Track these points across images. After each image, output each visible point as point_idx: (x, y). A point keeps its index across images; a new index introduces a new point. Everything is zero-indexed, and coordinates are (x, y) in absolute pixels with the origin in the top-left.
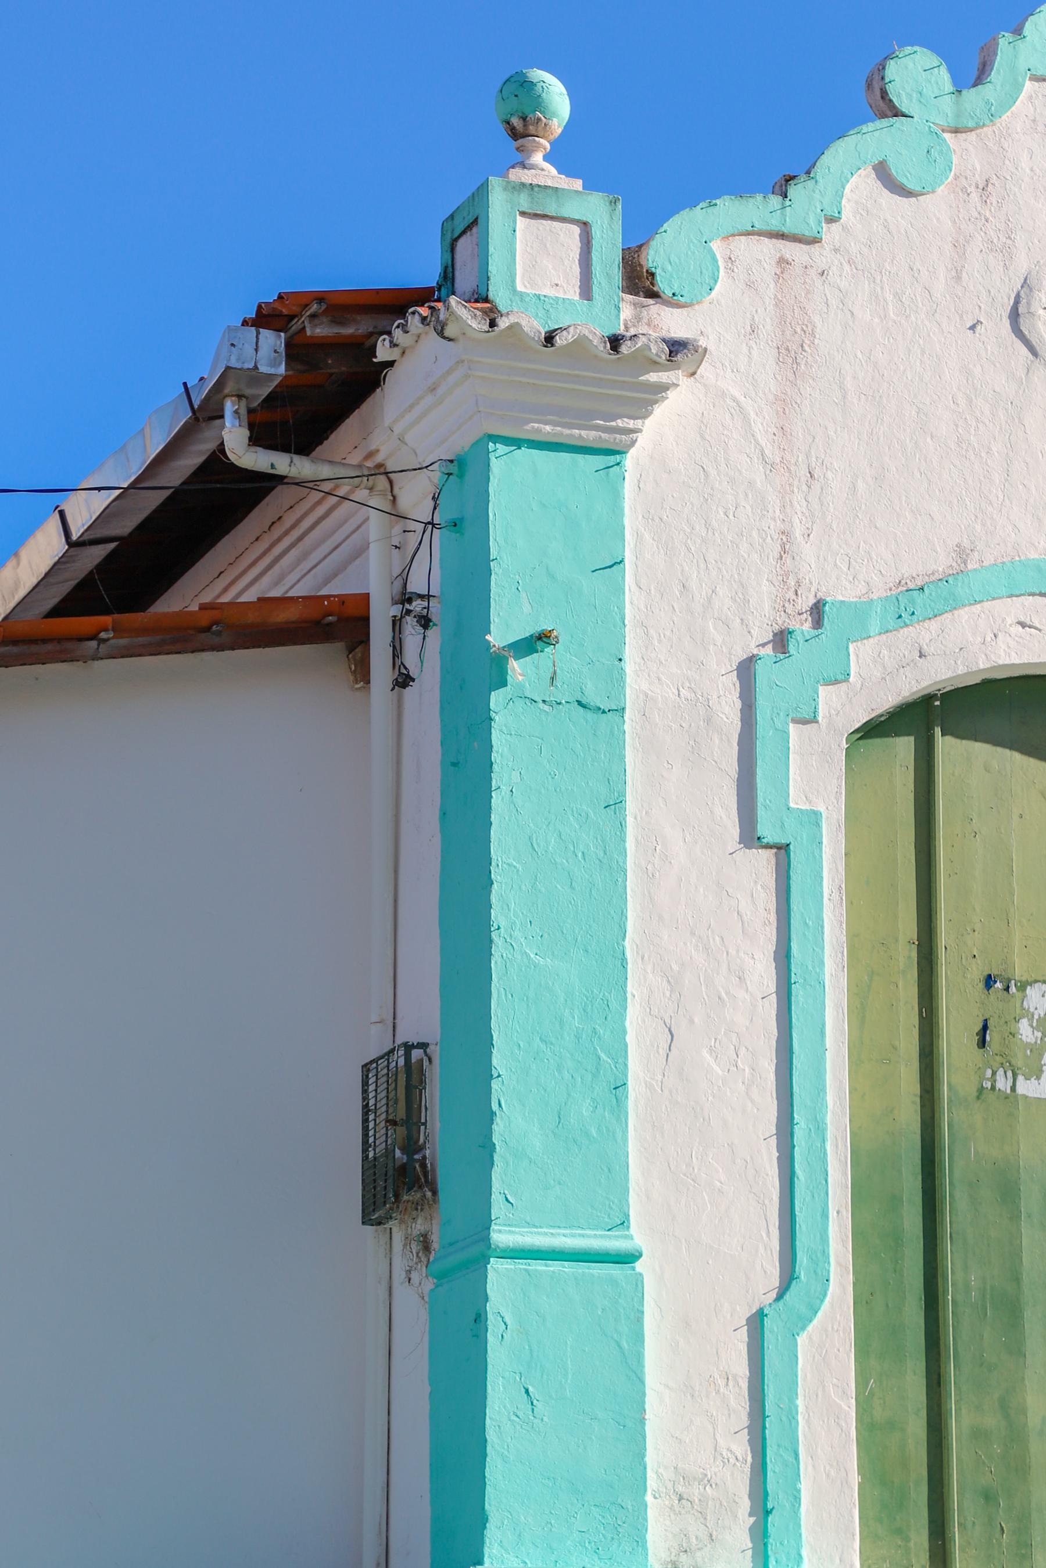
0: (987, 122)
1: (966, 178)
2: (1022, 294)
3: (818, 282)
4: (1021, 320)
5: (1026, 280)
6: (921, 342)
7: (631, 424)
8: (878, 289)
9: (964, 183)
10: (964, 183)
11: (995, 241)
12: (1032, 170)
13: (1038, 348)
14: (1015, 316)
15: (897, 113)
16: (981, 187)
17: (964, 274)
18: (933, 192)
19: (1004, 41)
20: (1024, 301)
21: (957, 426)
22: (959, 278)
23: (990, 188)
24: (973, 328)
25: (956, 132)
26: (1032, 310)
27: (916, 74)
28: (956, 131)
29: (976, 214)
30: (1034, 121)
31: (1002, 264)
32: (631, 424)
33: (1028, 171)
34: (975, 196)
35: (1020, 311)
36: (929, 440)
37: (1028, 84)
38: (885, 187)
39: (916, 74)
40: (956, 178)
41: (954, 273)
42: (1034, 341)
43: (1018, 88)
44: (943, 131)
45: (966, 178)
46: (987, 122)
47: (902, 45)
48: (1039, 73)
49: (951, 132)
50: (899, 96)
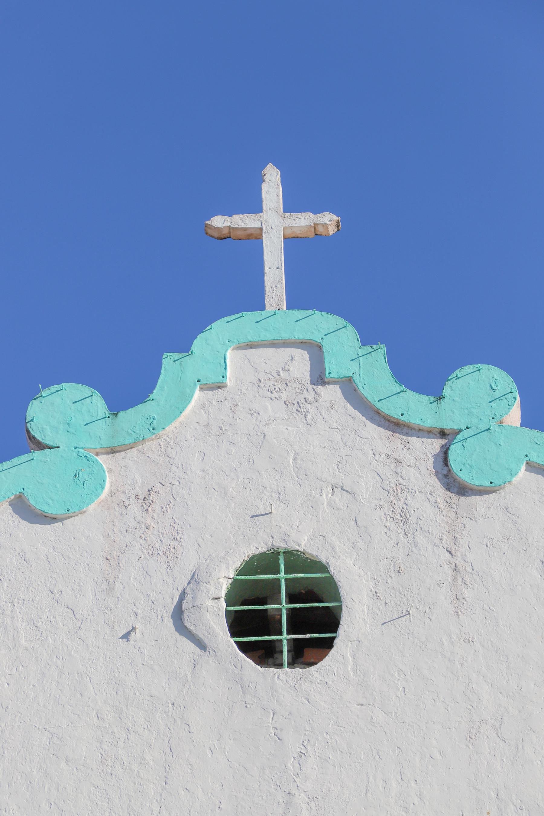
0: (148, 435)
1: (124, 493)
2: (188, 591)
3: (140, 553)
4: (185, 616)
5: (193, 575)
6: (59, 663)
7: (240, 577)
8: (9, 620)
9: (122, 497)
10: (122, 497)
11: (157, 545)
12: (203, 471)
13: (206, 641)
14: (178, 614)
15: (41, 446)
16: (141, 497)
17: (118, 585)
18: (82, 513)
19: (169, 361)
20: (188, 598)
21: (101, 742)
22: (110, 589)
23: (153, 496)
24: (126, 636)
25: (114, 452)
26: (198, 603)
27: (63, 410)
28: (113, 451)
29: (135, 524)
30: (207, 426)
31: (165, 566)
32: (240, 577)
33: (199, 473)
34: (135, 508)
35: (184, 607)
36: (63, 765)
37: (197, 393)
38: (23, 518)
39: (63, 410)
40: (112, 494)
41: (105, 586)
42: (200, 633)
43: (186, 398)
44: (97, 454)
45: (124, 493)
46: (148, 435)
47: (46, 386)
48: (210, 381)
49: (108, 453)
50: (42, 431)
